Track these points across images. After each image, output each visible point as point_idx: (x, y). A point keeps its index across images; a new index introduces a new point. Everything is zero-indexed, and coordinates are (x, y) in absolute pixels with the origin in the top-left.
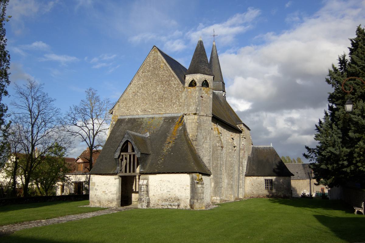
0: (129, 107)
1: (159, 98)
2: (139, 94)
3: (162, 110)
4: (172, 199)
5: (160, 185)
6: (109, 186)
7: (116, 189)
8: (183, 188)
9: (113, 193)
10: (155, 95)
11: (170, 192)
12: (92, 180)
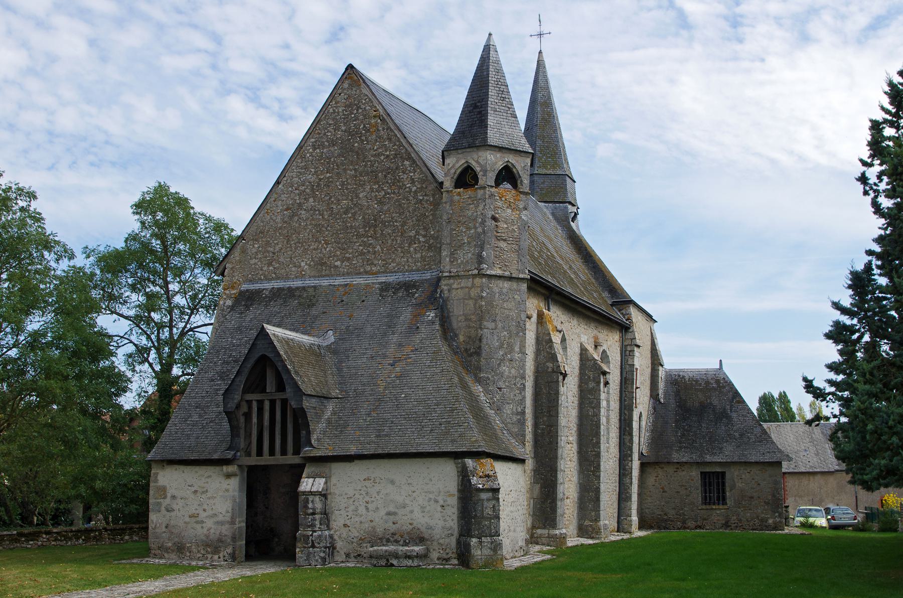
0: (274, 253)
1: (366, 224)
2: (303, 212)
5: (364, 493)
6: (209, 498)
7: (230, 505)
9: (220, 518)
10: (354, 214)
11: (395, 514)
12: (156, 481)
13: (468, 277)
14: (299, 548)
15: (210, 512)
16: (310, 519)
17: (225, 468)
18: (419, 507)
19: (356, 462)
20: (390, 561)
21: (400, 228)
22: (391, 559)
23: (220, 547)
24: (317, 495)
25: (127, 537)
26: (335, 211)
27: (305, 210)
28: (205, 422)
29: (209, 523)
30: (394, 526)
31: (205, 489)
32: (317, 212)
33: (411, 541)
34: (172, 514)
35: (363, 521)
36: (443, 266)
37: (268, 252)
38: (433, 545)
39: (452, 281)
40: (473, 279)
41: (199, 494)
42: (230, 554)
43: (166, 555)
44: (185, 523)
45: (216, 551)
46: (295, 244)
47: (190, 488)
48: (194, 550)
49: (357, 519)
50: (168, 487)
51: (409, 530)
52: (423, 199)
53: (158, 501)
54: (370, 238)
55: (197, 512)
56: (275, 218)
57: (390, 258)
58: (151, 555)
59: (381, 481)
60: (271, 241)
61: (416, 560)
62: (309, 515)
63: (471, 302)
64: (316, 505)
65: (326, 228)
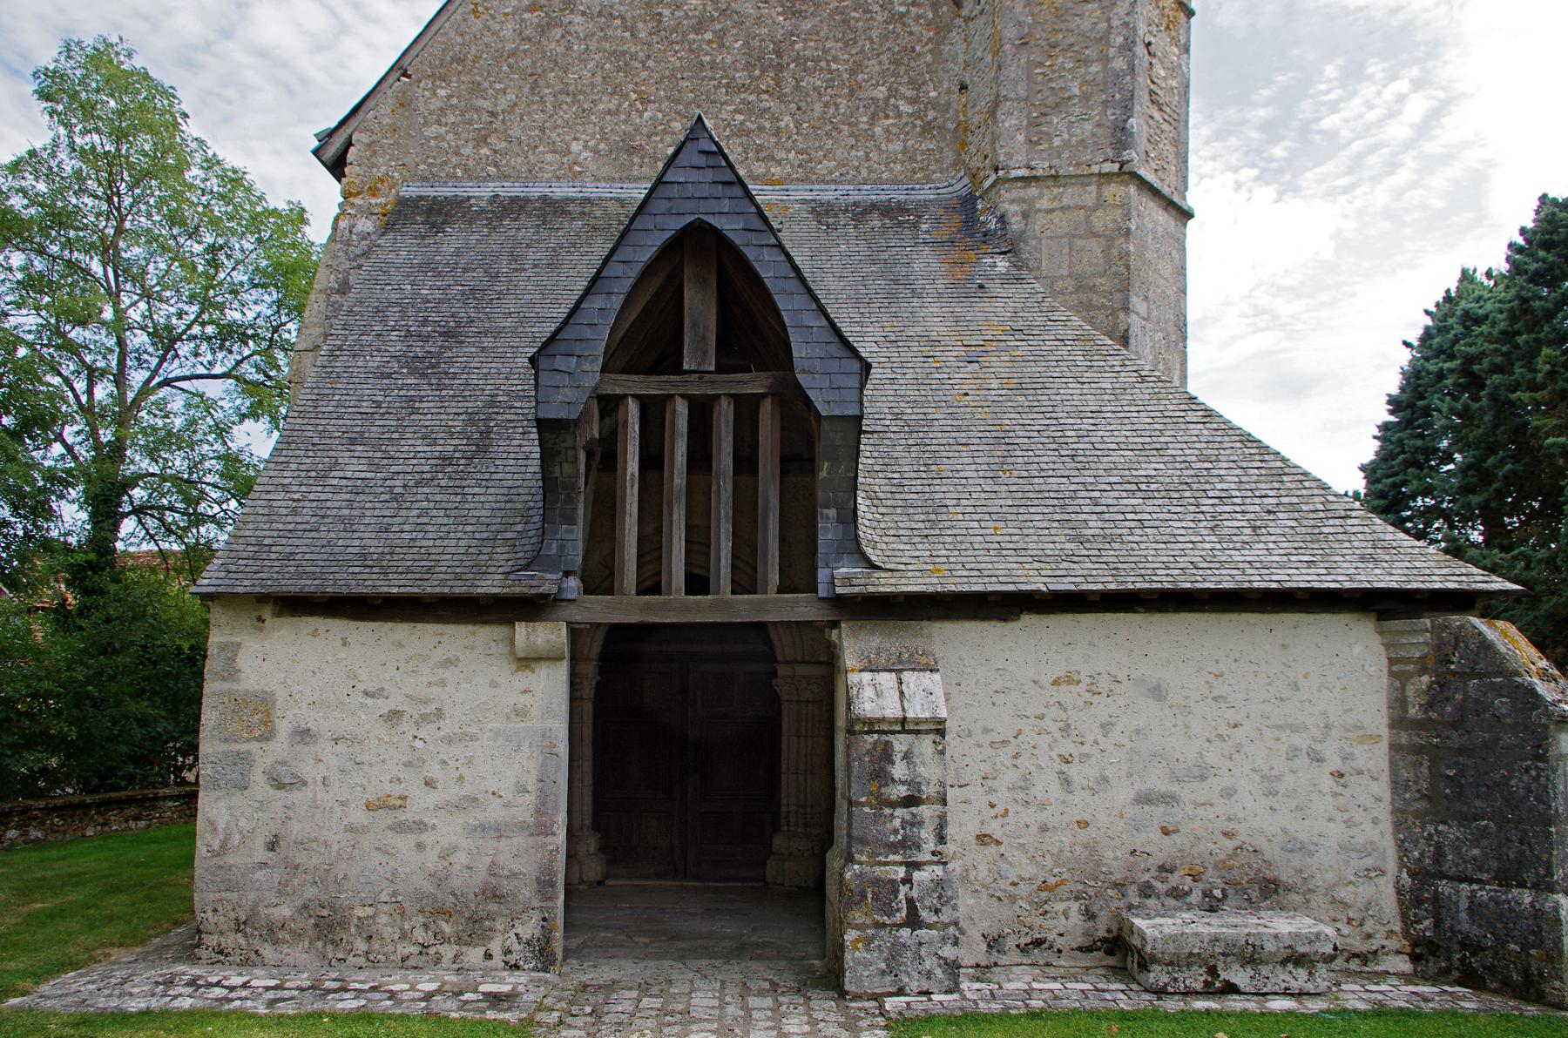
0: (493, 114)
1: (754, 59)
2: (578, 19)
3: (780, 155)
4: (1196, 878)
5: (1054, 728)
6: (449, 741)
7: (533, 766)
8: (1317, 758)
9: (494, 812)
10: (721, 35)
11: (1169, 799)
12: (232, 673)
13: (1082, 180)
14: (857, 927)
15: (449, 791)
16: (897, 823)
17: (521, 629)
18: (1257, 778)
19: (1027, 619)
20: (1223, 975)
21: (846, 76)
22: (1227, 968)
23: (490, 917)
24: (927, 732)
25: (12, 834)
26: (667, 21)
27: (584, 13)
28: (398, 483)
29: (449, 831)
30: (1167, 840)
31: (431, 708)
32: (618, 22)
33: (1230, 891)
34: (295, 796)
35: (1052, 822)
36: (1007, 154)
37: (477, 110)
38: (1313, 904)
39: (1033, 191)
40: (1100, 185)
41: (406, 725)
42: (528, 943)
43: (268, 951)
44: (350, 829)
45: (476, 930)
46: (555, 96)
47: (370, 701)
48: (385, 924)
49: (1031, 817)
50: (281, 695)
51: (1222, 857)
52: (908, 10)
53: (236, 747)
54: (765, 97)
55: (399, 790)
56: (497, 27)
57: (820, 148)
58: (202, 952)
59: (1117, 688)
60: (486, 84)
61: (1322, 970)
62: (893, 805)
63: (1095, 247)
64: (921, 769)
65: (643, 63)
